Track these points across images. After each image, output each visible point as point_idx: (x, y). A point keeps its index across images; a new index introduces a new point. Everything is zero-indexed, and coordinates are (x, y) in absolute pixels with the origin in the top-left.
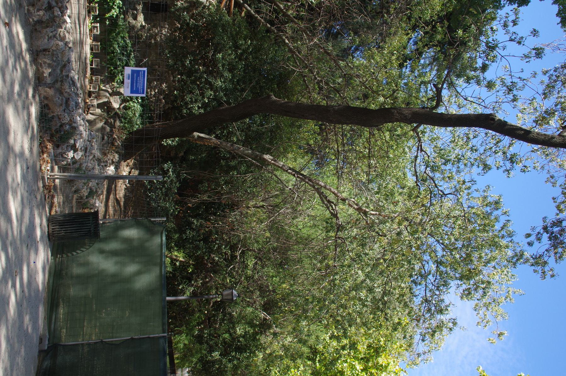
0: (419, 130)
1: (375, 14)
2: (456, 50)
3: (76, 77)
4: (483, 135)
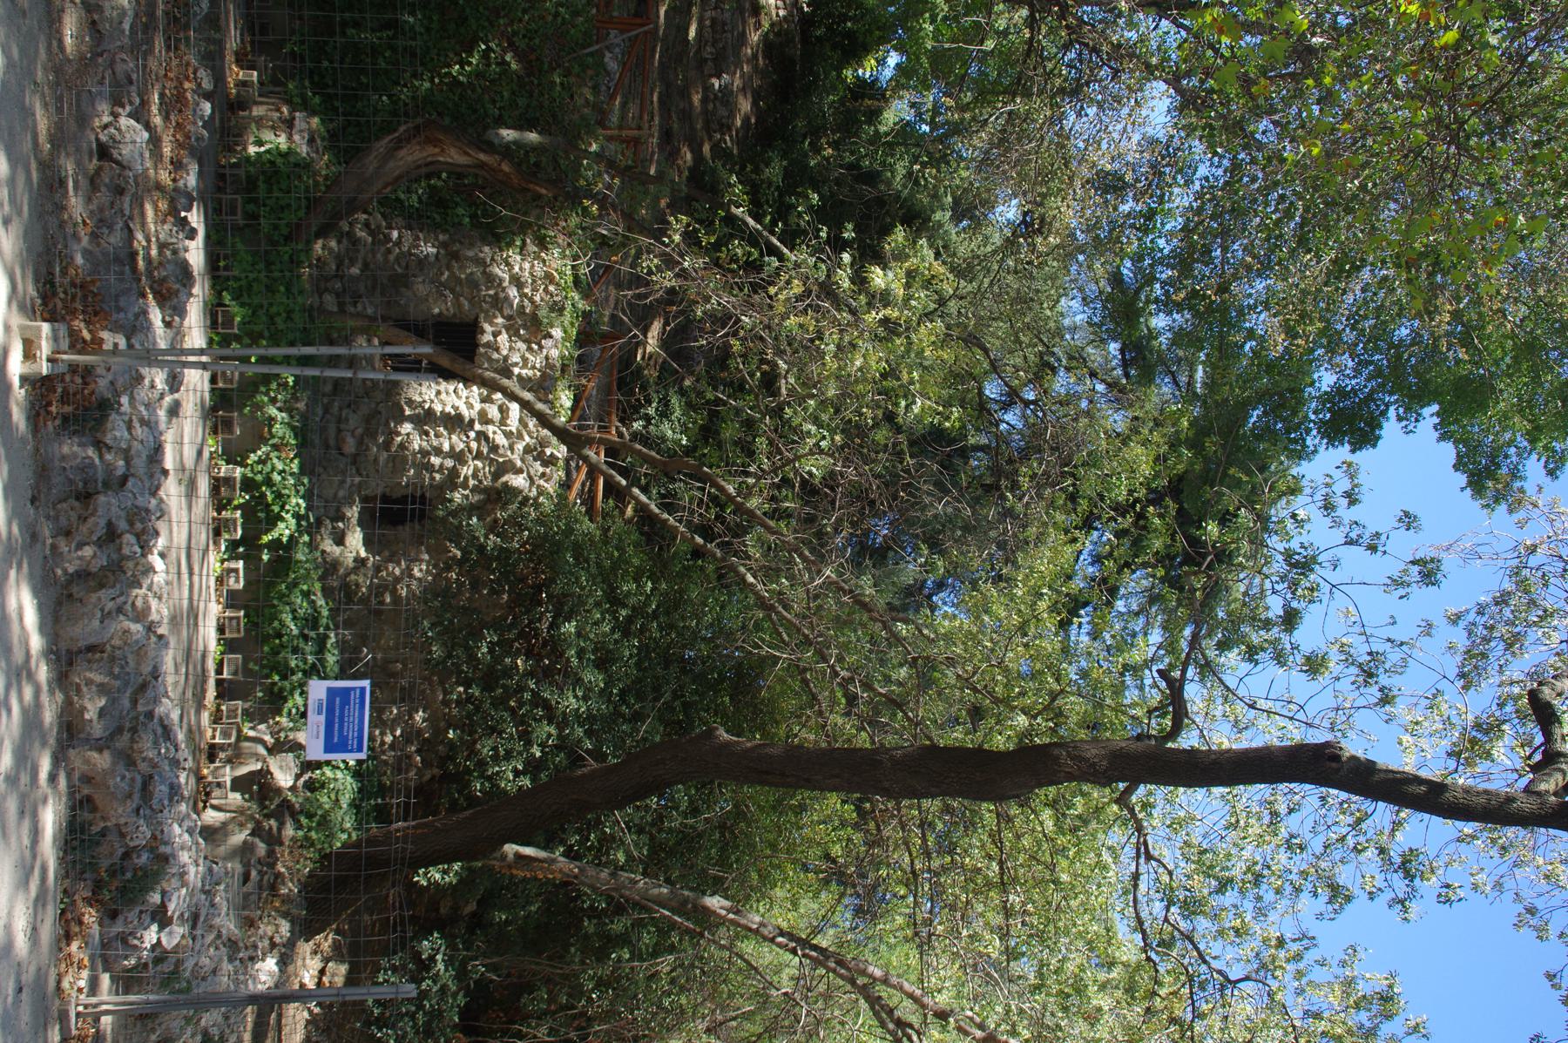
0: (1134, 799)
1: (979, 492)
2: (1209, 577)
3: (175, 715)
4: (1317, 803)
